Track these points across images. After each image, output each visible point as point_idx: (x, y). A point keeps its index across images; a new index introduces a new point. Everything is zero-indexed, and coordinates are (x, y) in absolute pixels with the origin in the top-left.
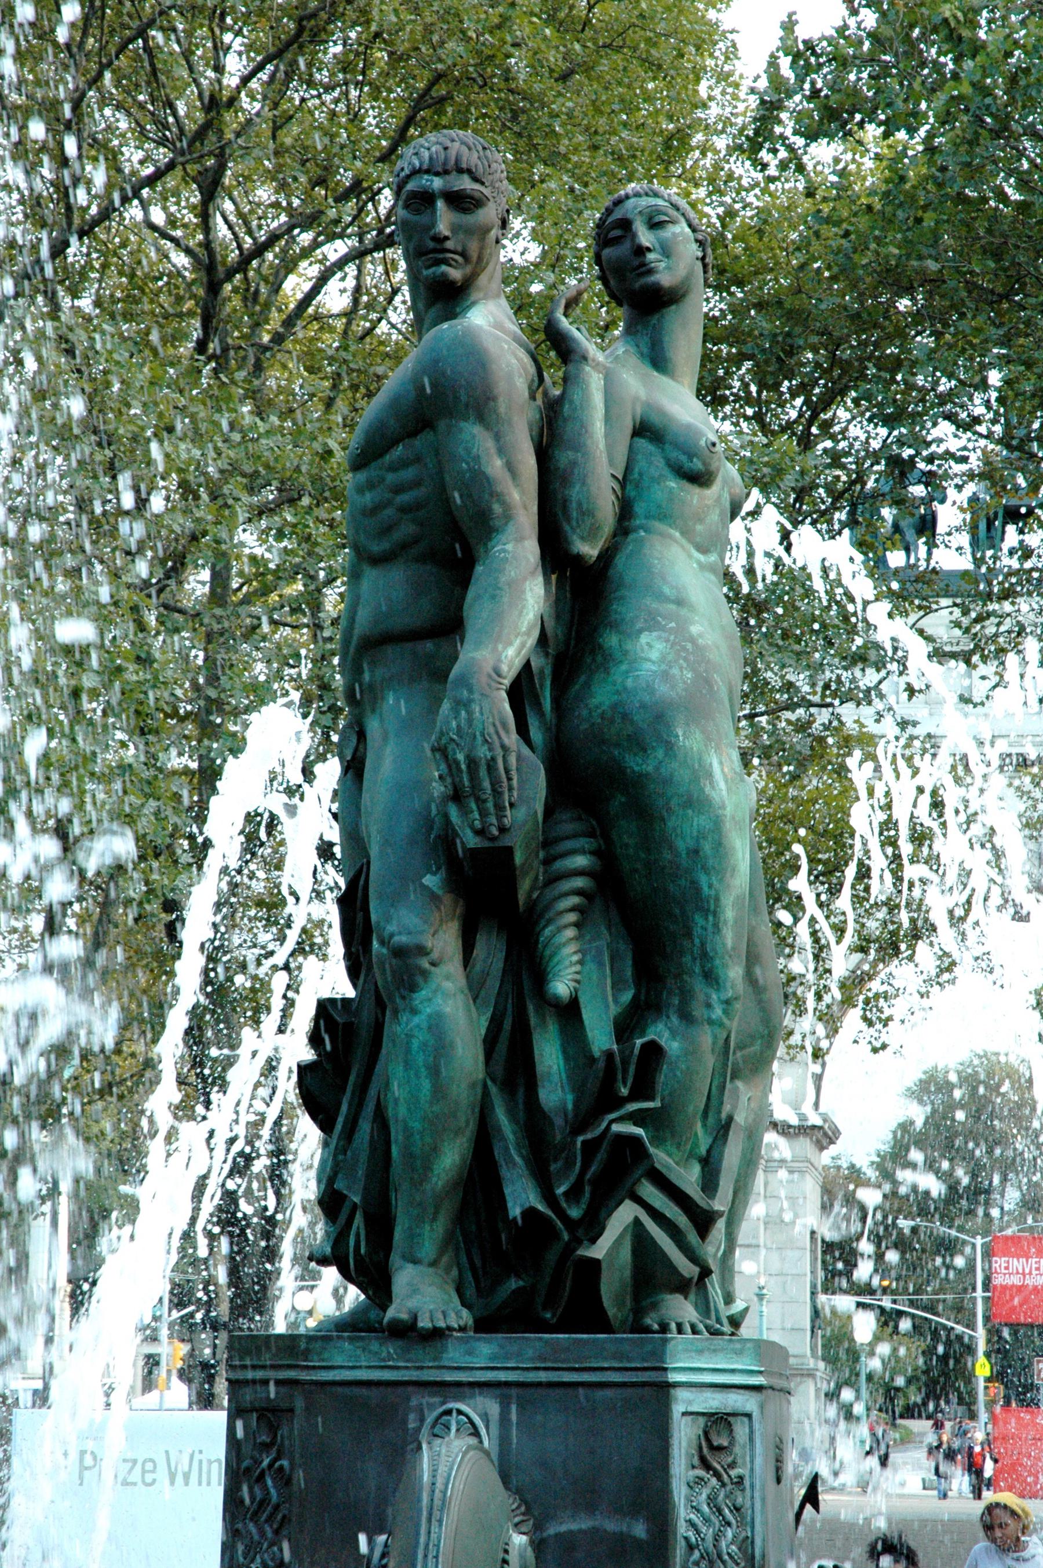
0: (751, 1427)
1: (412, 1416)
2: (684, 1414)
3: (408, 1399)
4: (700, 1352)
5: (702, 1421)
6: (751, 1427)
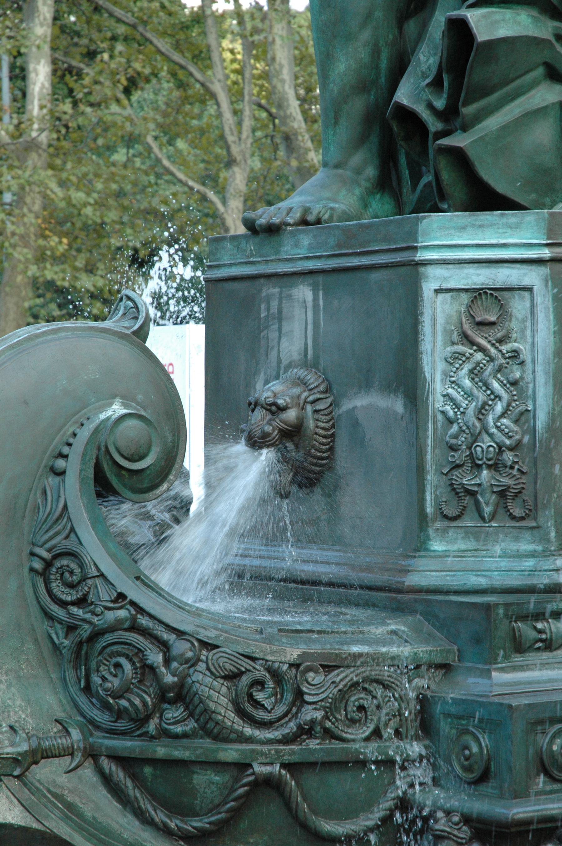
0: (532, 301)
1: (263, 306)
3: (260, 291)
4: (463, 228)
5: (465, 298)
6: (532, 301)
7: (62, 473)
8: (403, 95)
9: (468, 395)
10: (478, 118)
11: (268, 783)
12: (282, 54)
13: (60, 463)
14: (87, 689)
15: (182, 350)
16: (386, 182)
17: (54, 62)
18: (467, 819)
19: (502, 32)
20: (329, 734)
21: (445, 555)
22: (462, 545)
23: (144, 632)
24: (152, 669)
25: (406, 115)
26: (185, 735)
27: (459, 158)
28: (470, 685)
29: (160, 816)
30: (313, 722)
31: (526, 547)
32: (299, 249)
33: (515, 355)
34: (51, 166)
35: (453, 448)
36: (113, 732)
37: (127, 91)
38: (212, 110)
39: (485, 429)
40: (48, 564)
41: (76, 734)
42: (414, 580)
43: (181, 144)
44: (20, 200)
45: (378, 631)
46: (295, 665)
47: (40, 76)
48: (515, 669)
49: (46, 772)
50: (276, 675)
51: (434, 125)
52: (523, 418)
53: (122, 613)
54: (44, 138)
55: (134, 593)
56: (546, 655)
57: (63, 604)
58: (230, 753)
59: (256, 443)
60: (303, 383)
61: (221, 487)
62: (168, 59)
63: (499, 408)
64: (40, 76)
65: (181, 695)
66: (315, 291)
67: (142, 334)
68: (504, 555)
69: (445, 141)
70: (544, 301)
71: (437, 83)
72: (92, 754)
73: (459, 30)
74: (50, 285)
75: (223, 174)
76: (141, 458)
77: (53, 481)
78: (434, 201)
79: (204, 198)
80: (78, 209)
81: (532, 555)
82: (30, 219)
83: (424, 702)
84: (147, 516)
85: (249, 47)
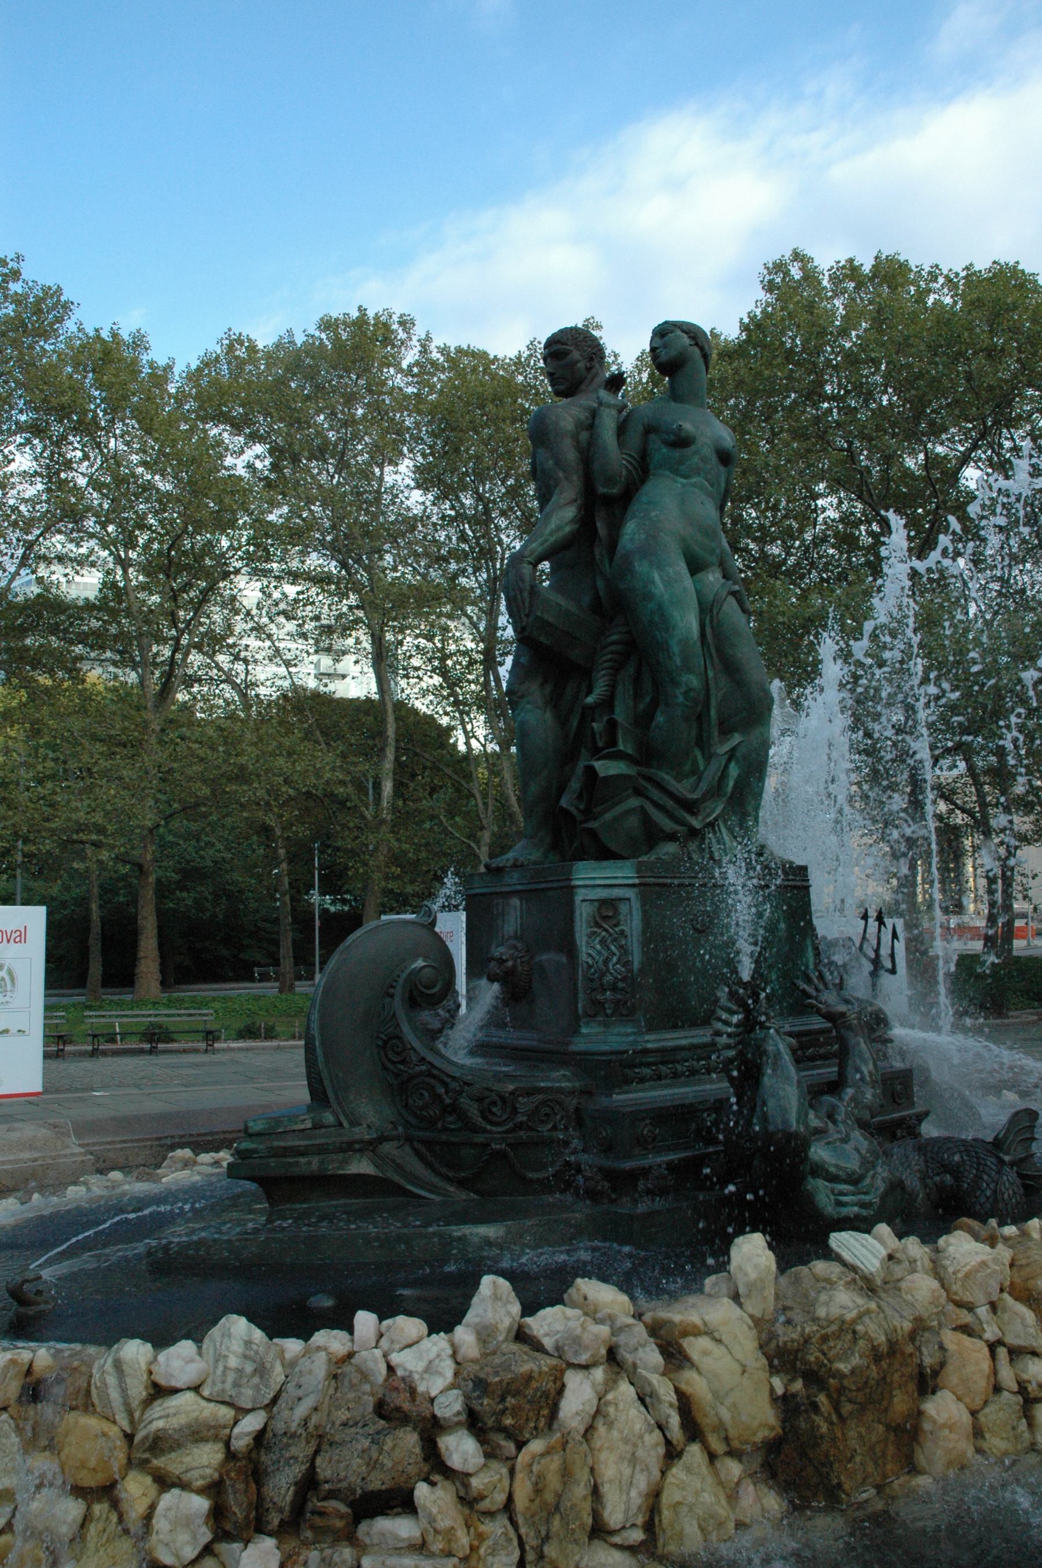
2: (584, 901)
5: (596, 904)
7: (392, 996)
8: (564, 802)
9: (599, 953)
10: (601, 814)
11: (501, 1155)
12: (507, 775)
13: (392, 990)
14: (406, 1106)
15: (453, 928)
16: (555, 846)
17: (394, 780)
18: (601, 1169)
19: (612, 772)
20: (531, 1129)
21: (588, 1035)
22: (597, 1030)
23: (435, 1077)
24: (440, 1096)
25: (565, 812)
26: (456, 1130)
27: (592, 833)
28: (603, 1102)
29: (444, 1170)
30: (521, 1123)
31: (629, 1030)
32: (513, 880)
33: (622, 932)
34: (392, 832)
35: (592, 980)
36: (421, 1129)
37: (431, 794)
38: (473, 803)
39: (608, 970)
40: (385, 1042)
41: (400, 1129)
42: (573, 1048)
43: (457, 819)
44: (376, 849)
45: (555, 1074)
46: (512, 1093)
47: (388, 788)
48: (626, 1092)
49: (387, 1148)
50: (502, 1098)
51: (579, 817)
52: (627, 964)
53: (424, 1068)
54: (389, 818)
55: (430, 1057)
56: (640, 1086)
57: (394, 1063)
58: (479, 1139)
59: (492, 979)
60: (515, 947)
61: (474, 1003)
62: (450, 777)
63: (615, 959)
64: (388, 788)
65: (454, 1109)
66: (521, 900)
67: (433, 924)
68: (619, 1035)
69: (585, 825)
70: (636, 904)
71: (580, 797)
72: (409, 1139)
73: (591, 771)
74: (391, 891)
75: (479, 834)
76: (434, 987)
77: (388, 1000)
78: (581, 855)
79: (469, 846)
80: (405, 853)
81: (634, 1034)
82: (382, 858)
83: (577, 1110)
84: (437, 1015)
85: (492, 772)
